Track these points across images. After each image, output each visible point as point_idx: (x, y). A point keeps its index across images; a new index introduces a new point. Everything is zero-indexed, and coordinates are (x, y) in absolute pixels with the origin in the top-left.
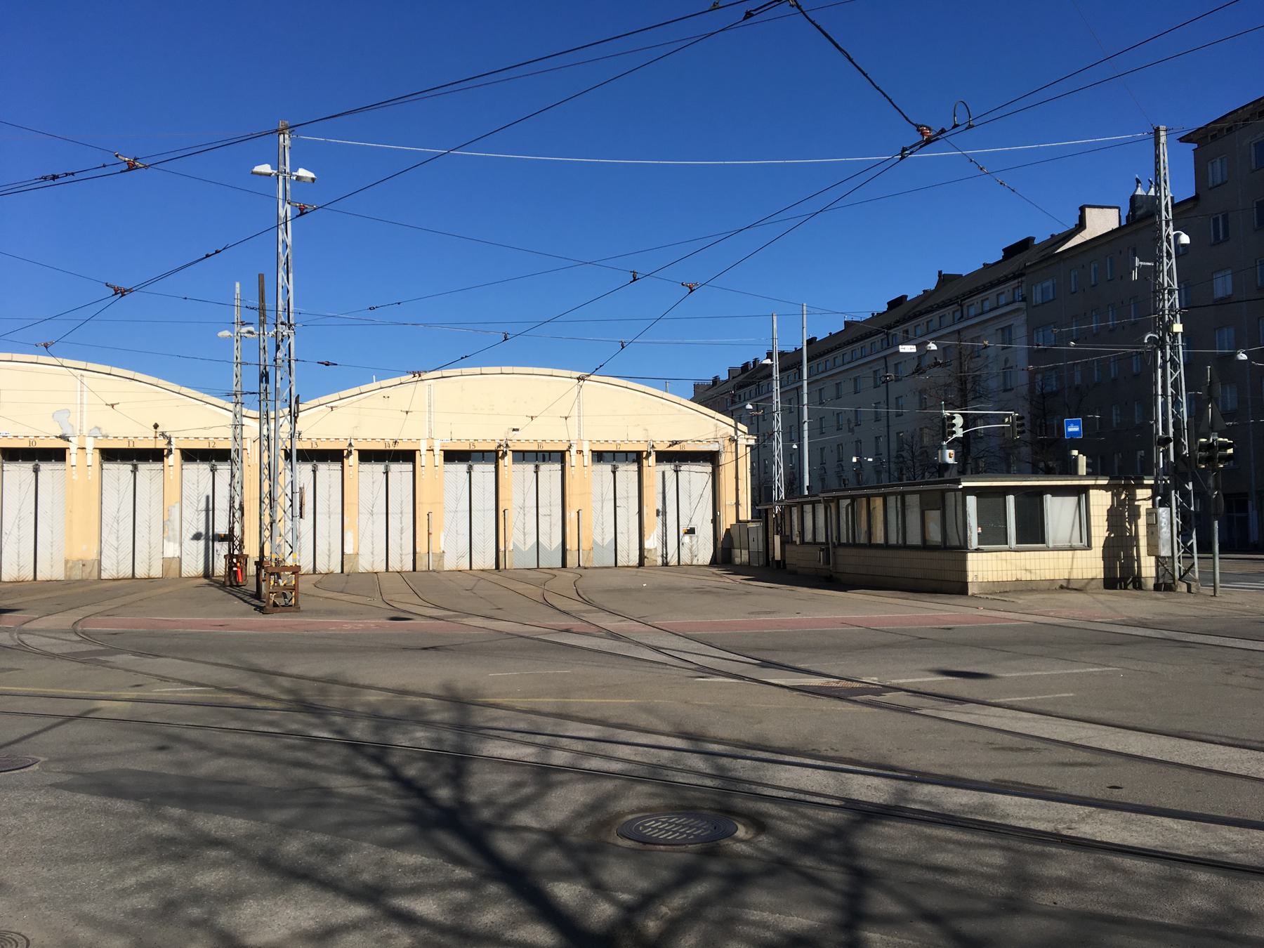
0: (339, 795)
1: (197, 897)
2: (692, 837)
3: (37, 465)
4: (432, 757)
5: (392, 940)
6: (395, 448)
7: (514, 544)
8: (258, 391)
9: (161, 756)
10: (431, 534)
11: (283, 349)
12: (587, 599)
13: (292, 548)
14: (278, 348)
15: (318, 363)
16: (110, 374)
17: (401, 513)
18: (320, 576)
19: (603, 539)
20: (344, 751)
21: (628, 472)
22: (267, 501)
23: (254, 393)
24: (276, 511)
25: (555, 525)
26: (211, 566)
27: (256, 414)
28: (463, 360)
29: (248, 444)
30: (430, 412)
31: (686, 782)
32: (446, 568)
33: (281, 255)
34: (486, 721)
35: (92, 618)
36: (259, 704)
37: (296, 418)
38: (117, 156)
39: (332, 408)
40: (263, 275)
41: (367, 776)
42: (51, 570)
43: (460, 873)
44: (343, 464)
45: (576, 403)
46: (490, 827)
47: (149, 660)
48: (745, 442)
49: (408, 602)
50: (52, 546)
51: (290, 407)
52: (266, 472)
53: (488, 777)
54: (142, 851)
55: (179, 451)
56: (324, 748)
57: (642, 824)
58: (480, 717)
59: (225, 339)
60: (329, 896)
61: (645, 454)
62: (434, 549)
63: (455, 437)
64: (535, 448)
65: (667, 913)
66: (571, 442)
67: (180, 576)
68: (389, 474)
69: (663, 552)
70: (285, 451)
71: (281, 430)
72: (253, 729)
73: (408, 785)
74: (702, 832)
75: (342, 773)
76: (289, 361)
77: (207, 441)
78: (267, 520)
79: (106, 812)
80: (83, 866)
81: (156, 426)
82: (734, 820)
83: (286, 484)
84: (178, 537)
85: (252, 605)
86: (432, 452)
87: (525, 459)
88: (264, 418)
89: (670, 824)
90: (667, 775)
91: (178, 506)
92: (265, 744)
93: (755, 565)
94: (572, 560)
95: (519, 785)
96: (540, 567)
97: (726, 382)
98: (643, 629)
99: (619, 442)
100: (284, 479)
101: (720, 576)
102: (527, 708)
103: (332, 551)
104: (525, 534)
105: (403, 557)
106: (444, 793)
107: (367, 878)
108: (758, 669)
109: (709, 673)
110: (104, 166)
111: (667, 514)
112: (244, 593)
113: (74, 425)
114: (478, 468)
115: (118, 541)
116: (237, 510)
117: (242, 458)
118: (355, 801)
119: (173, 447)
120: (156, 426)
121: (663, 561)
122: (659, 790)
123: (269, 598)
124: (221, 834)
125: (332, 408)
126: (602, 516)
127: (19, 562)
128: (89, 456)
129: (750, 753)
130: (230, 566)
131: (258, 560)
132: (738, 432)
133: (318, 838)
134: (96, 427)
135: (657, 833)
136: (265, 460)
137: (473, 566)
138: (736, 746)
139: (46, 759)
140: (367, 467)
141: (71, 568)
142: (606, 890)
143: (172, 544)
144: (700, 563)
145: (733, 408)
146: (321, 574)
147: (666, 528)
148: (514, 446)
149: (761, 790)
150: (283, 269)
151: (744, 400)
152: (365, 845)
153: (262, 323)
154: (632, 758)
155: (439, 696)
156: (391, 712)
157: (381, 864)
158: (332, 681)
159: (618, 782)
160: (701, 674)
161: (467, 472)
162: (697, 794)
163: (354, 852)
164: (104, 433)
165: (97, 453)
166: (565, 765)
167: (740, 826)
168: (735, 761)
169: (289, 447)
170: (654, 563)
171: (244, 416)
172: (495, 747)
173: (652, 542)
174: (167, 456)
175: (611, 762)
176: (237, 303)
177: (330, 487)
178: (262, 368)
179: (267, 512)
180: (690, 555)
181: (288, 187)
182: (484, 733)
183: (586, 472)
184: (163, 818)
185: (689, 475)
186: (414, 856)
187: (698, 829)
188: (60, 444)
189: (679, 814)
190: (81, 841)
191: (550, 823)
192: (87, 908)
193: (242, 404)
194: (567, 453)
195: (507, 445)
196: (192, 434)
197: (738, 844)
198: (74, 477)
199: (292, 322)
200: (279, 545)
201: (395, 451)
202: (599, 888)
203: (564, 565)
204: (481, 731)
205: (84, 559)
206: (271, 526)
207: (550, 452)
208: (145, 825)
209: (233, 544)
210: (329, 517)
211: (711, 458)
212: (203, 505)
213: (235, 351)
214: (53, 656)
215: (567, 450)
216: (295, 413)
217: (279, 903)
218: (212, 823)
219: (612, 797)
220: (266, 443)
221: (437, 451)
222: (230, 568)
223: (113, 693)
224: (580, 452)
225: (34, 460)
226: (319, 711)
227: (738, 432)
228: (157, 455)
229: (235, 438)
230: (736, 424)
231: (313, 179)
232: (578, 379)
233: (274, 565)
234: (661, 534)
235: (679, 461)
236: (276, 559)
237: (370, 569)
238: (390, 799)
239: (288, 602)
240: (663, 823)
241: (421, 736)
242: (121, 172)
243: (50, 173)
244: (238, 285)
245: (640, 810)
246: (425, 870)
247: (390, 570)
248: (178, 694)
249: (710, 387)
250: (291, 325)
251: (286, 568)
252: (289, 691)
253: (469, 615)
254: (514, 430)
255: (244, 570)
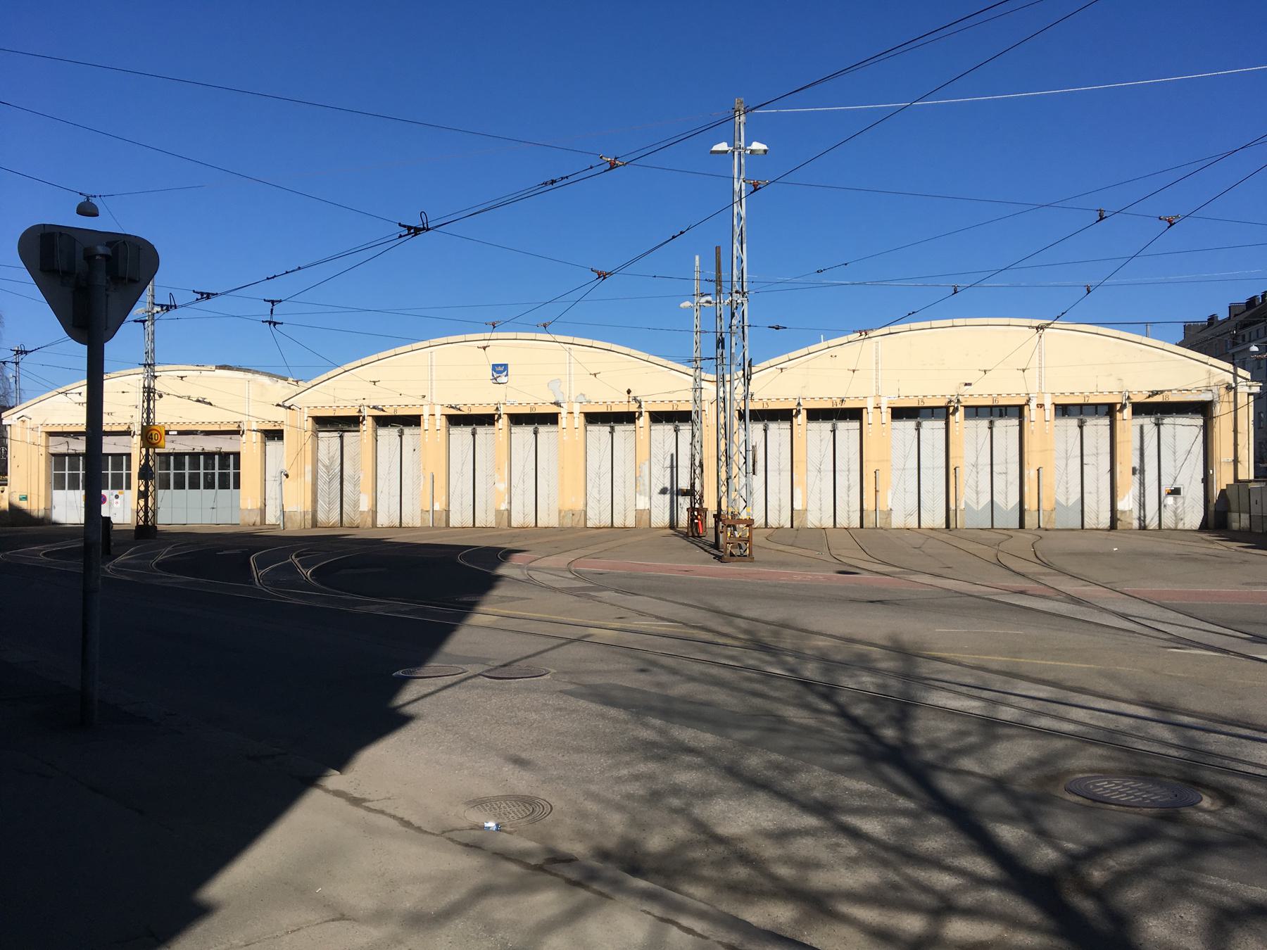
0: (793, 724)
1: (676, 791)
2: (1149, 801)
3: (536, 428)
4: (877, 700)
5: (840, 848)
6: (843, 407)
7: (966, 502)
8: (715, 357)
9: (642, 676)
10: (878, 491)
11: (738, 316)
12: (1046, 562)
13: (746, 502)
14: (733, 315)
15: (769, 327)
16: (591, 347)
17: (849, 470)
18: (772, 530)
19: (1067, 499)
20: (797, 687)
21: (1097, 428)
22: (723, 459)
23: (711, 359)
24: (732, 468)
25: (1011, 483)
26: (675, 518)
27: (713, 377)
28: (911, 316)
29: (706, 406)
30: (877, 370)
31: (1148, 749)
32: (894, 526)
33: (736, 227)
34: (932, 673)
35: (582, 559)
36: (721, 640)
37: (749, 380)
38: (601, 157)
39: (782, 369)
40: (719, 247)
41: (817, 711)
42: (548, 519)
43: (903, 803)
44: (792, 422)
45: (1037, 350)
46: (933, 767)
47: (629, 597)
48: (1247, 390)
49: (854, 557)
50: (549, 497)
51: (744, 370)
52: (723, 431)
53: (932, 723)
54: (632, 750)
55: (648, 413)
56: (778, 683)
57: (1093, 784)
58: (925, 669)
59: (686, 309)
60: (784, 805)
61: (1118, 407)
62: (881, 506)
63: (902, 394)
64: (990, 403)
65: (1115, 866)
66: (1030, 395)
67: (650, 527)
68: (837, 431)
69: (1140, 515)
70: (739, 411)
71: (736, 391)
72: (716, 661)
73: (854, 722)
74: (1160, 798)
75: (794, 705)
76: (743, 328)
77: (671, 404)
78: (723, 476)
79: (603, 716)
80: (588, 756)
81: (629, 392)
82: (1200, 791)
83: (740, 443)
84: (648, 490)
85: (711, 554)
86: (879, 409)
87: (979, 414)
88: (720, 381)
89: (1124, 787)
90: (1126, 741)
91: (647, 463)
92: (726, 674)
93: (1257, 531)
94: (1030, 521)
95: (963, 734)
96: (995, 527)
97: (1224, 321)
98: (1109, 595)
99: (1088, 394)
100: (739, 437)
101: (1211, 542)
102: (974, 664)
103: (782, 506)
104: (977, 493)
105: (851, 514)
106: (889, 733)
107: (818, 795)
108: (1248, 644)
109: (1186, 645)
110: (591, 168)
111: (1146, 473)
112: (704, 543)
113: (564, 392)
114: (927, 425)
115: (599, 494)
116: (697, 467)
117: (701, 419)
118: (806, 730)
119: (643, 410)
120: (629, 392)
121: (1140, 524)
122: (1116, 754)
123: (726, 549)
124: (693, 744)
125: (782, 369)
126: (1067, 474)
127: (524, 511)
128: (576, 419)
129: (1226, 728)
130: (692, 519)
131: (716, 513)
132: (1238, 378)
133: (775, 757)
134: (581, 394)
135: (1108, 793)
136: (722, 421)
137: (922, 525)
138: (1210, 720)
139: (555, 671)
140: (815, 426)
141: (563, 517)
142: (1051, 837)
143: (643, 497)
144: (1187, 527)
145: (1235, 350)
146: (772, 528)
147: (1144, 488)
148: (966, 401)
149: (1233, 765)
150: (738, 240)
151: (1250, 342)
152: (816, 768)
153: (719, 292)
154: (1087, 721)
155: (885, 646)
156: (839, 657)
157: (830, 785)
158: (785, 625)
159: (1069, 742)
160: (1175, 645)
161: (916, 429)
162: (1158, 762)
163: (807, 772)
164: (588, 399)
165: (582, 417)
166: (1013, 721)
167: (1205, 797)
168: (1207, 734)
169: (743, 408)
170: (1130, 526)
171: (703, 380)
172: (940, 697)
173: (1127, 503)
174: (638, 418)
175: (1062, 722)
176: (697, 275)
177: (780, 445)
178: (718, 334)
179: (724, 469)
180: (1174, 518)
181: (743, 161)
182: (929, 683)
183: (1047, 428)
184: (646, 725)
185: (1174, 429)
186: (860, 783)
187: (1156, 794)
188: (554, 409)
189: (1136, 778)
190: (585, 737)
191: (994, 771)
192: (593, 788)
193: (701, 368)
194: (1026, 408)
195: (958, 400)
196: (658, 398)
197: (1200, 814)
198: (565, 438)
199: (745, 290)
200: (734, 500)
201: (842, 409)
202: (1043, 834)
203: (1022, 525)
204: (926, 682)
205: (573, 509)
206: (727, 482)
207: (1006, 407)
208: (633, 730)
209: (695, 498)
210: (780, 474)
211: (1203, 409)
212: (668, 463)
213: (695, 320)
214: (554, 589)
215: (1026, 404)
216: (748, 375)
217: (743, 804)
218: (687, 735)
219: (1064, 754)
220: (722, 405)
221: (884, 409)
222: (692, 520)
223: (602, 623)
224: (1041, 406)
225: (472, 425)
226: (773, 651)
227: (1238, 378)
228: (629, 418)
229: (695, 401)
230: (1235, 369)
231: (765, 151)
232: (1037, 328)
233: (730, 517)
234: (1138, 494)
235: (1161, 414)
236: (732, 513)
237: (818, 525)
238: (837, 730)
239: (742, 552)
240: (1117, 785)
241: (867, 681)
242: (605, 171)
243: (549, 179)
244: (697, 258)
245: (1092, 771)
246: (872, 796)
247: (838, 526)
248: (653, 628)
249: (1204, 328)
250: (744, 293)
251: (741, 521)
252: (746, 631)
253: (917, 572)
254: (966, 385)
255: (704, 522)
